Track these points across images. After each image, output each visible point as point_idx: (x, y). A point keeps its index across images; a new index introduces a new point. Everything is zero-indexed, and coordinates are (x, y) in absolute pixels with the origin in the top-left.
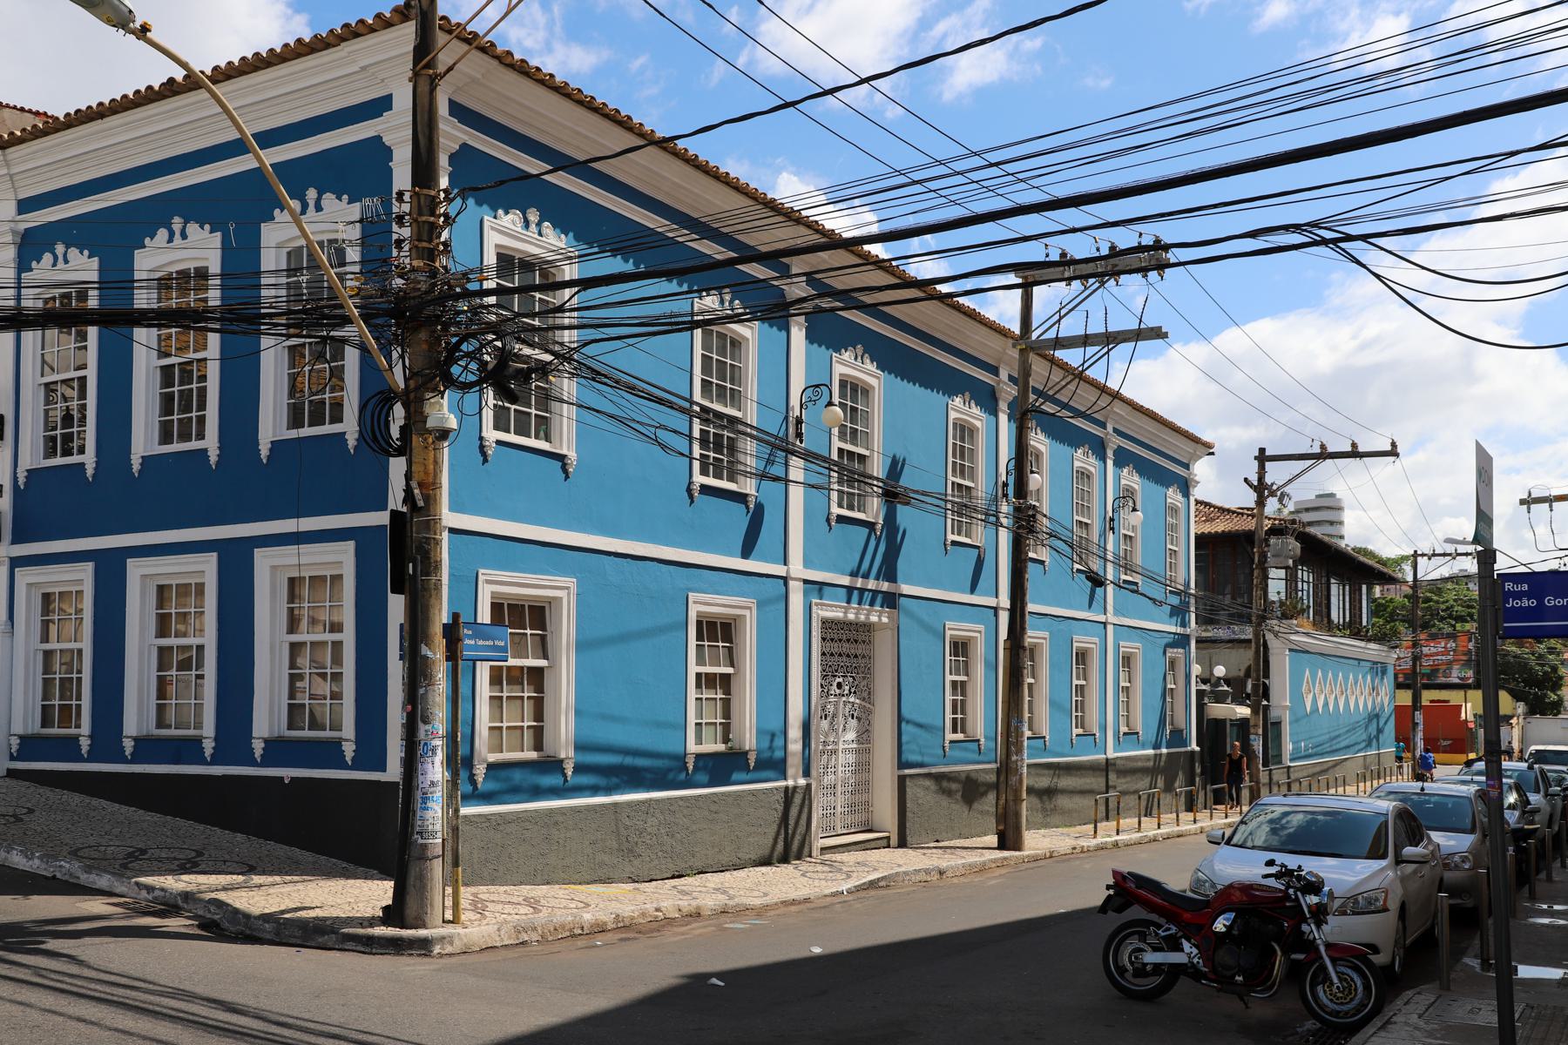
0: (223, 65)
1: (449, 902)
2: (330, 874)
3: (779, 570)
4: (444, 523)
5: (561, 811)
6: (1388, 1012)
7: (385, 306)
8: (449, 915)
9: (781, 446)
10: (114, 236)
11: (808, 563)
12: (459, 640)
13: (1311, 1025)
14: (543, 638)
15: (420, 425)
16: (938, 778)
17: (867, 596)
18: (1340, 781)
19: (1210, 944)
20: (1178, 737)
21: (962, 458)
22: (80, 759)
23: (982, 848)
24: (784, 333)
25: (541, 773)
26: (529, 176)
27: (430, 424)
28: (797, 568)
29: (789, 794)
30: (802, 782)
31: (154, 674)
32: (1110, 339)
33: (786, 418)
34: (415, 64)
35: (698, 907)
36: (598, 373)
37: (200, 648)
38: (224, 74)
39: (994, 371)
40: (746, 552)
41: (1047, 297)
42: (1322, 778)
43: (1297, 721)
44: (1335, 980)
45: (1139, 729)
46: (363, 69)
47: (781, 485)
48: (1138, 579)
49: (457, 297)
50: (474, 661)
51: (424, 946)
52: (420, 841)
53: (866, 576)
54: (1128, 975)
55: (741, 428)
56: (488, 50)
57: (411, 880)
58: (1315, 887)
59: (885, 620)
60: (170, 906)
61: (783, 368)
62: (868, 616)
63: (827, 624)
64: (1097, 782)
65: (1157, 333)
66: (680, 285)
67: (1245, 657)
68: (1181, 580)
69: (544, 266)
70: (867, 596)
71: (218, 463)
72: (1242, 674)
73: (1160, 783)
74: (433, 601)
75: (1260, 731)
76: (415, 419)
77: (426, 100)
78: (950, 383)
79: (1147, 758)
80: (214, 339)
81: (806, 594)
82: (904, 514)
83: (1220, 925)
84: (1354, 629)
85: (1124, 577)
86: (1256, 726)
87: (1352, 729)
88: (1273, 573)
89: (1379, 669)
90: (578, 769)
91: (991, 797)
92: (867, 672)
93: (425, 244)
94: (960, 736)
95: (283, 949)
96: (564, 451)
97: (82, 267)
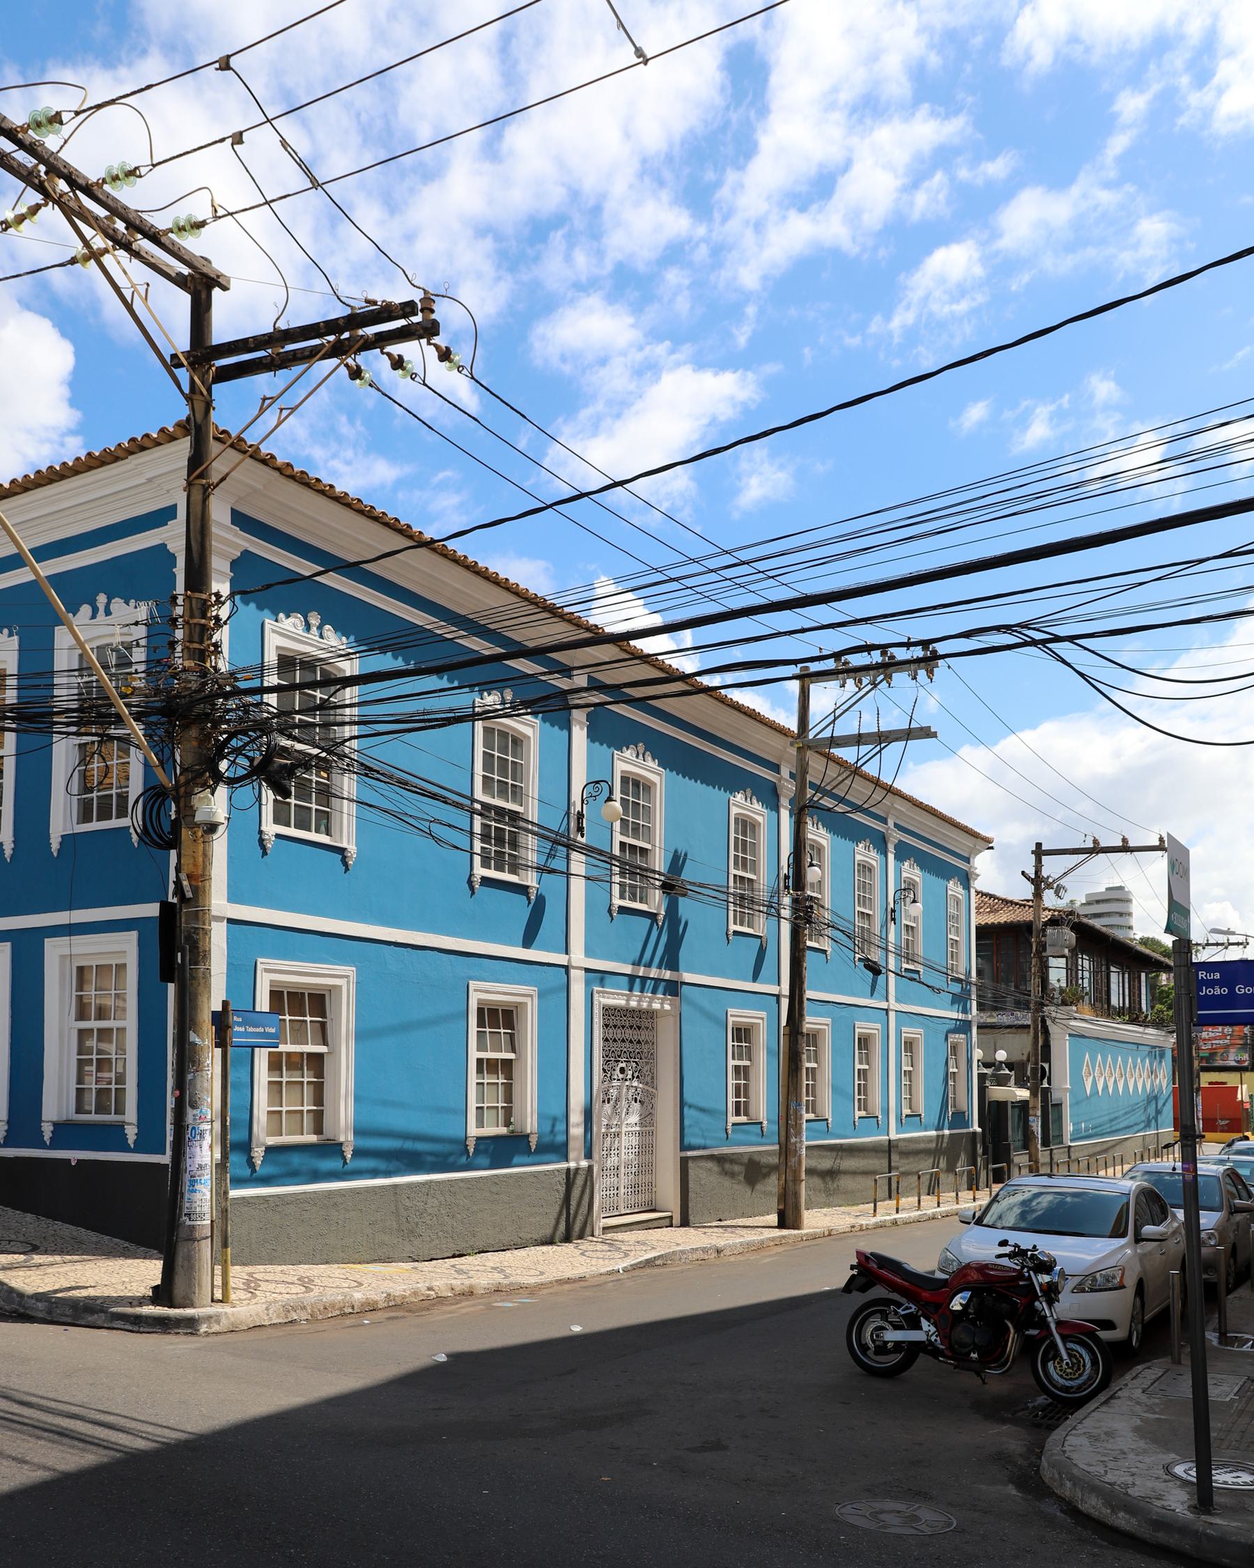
1: (218, 1281)
2: (110, 1253)
3: (561, 959)
5: (340, 1193)
6: (1114, 1386)
7: (156, 704)
8: (218, 1295)
9: (560, 842)
11: (589, 952)
13: (1042, 1400)
14: (323, 1025)
15: (189, 819)
16: (720, 1160)
17: (650, 984)
18: (1118, 1160)
19: (948, 1322)
20: (960, 1118)
23: (761, 1226)
24: (565, 733)
25: (323, 1155)
27: (199, 818)
28: (578, 956)
29: (570, 1176)
30: (584, 1164)
32: (882, 738)
33: (568, 813)
34: (189, 475)
35: (471, 1286)
36: (371, 769)
39: (776, 768)
40: (528, 942)
41: (824, 697)
42: (1102, 1157)
43: (1077, 1103)
44: (1065, 1356)
45: (922, 1111)
46: (150, 480)
48: (920, 968)
49: (227, 696)
50: (253, 1047)
51: (190, 1325)
52: (188, 1223)
53: (649, 965)
54: (870, 1353)
55: (522, 824)
56: (255, 455)
57: (180, 1260)
58: (1046, 1266)
59: (667, 1007)
61: (564, 764)
62: (650, 1003)
63: (607, 1010)
64: (879, 1163)
65: (926, 733)
66: (450, 680)
67: (1021, 1045)
68: (962, 969)
70: (650, 984)
71: (12, 857)
72: (1025, 1058)
73: (943, 1164)
74: (201, 988)
75: (1039, 1113)
76: (187, 811)
77: (199, 508)
78: (732, 780)
79: (929, 1140)
81: (588, 983)
82: (686, 907)
83: (957, 1304)
84: (1133, 1015)
85: (905, 966)
86: (1034, 1108)
87: (1132, 1111)
88: (1053, 962)
89: (1156, 1052)
90: (358, 1153)
91: (773, 1179)
92: (652, 1057)
93: (196, 646)
94: (743, 1119)
95: (51, 1327)
96: (344, 845)
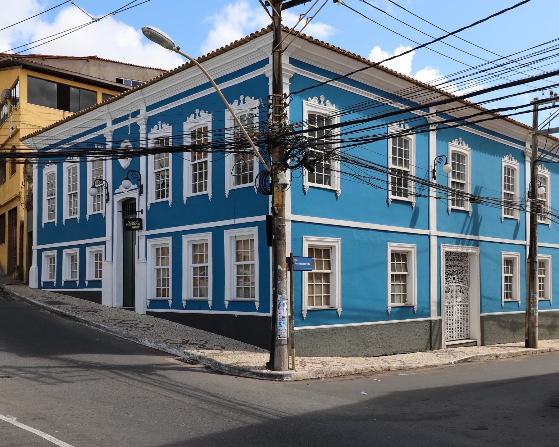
0: (211, 52)
1: (290, 362)
4: (286, 218)
7: (263, 139)
8: (291, 367)
9: (424, 183)
10: (176, 117)
11: (438, 229)
12: (293, 263)
14: (329, 262)
21: (509, 182)
22: (169, 308)
26: (323, 84)
28: (434, 231)
31: (192, 277)
33: (429, 171)
34: (273, 48)
35: (389, 367)
36: (346, 158)
37: (207, 267)
38: (203, 60)
39: (524, 144)
46: (258, 49)
47: (427, 199)
49: (289, 134)
51: (281, 377)
52: (279, 338)
56: (303, 37)
60: (195, 361)
61: (427, 151)
63: (447, 253)
66: (382, 121)
69: (328, 119)
77: (277, 61)
80: (210, 155)
92: (467, 273)
94: (509, 300)
95: (231, 377)
96: (336, 189)
97: (166, 130)
